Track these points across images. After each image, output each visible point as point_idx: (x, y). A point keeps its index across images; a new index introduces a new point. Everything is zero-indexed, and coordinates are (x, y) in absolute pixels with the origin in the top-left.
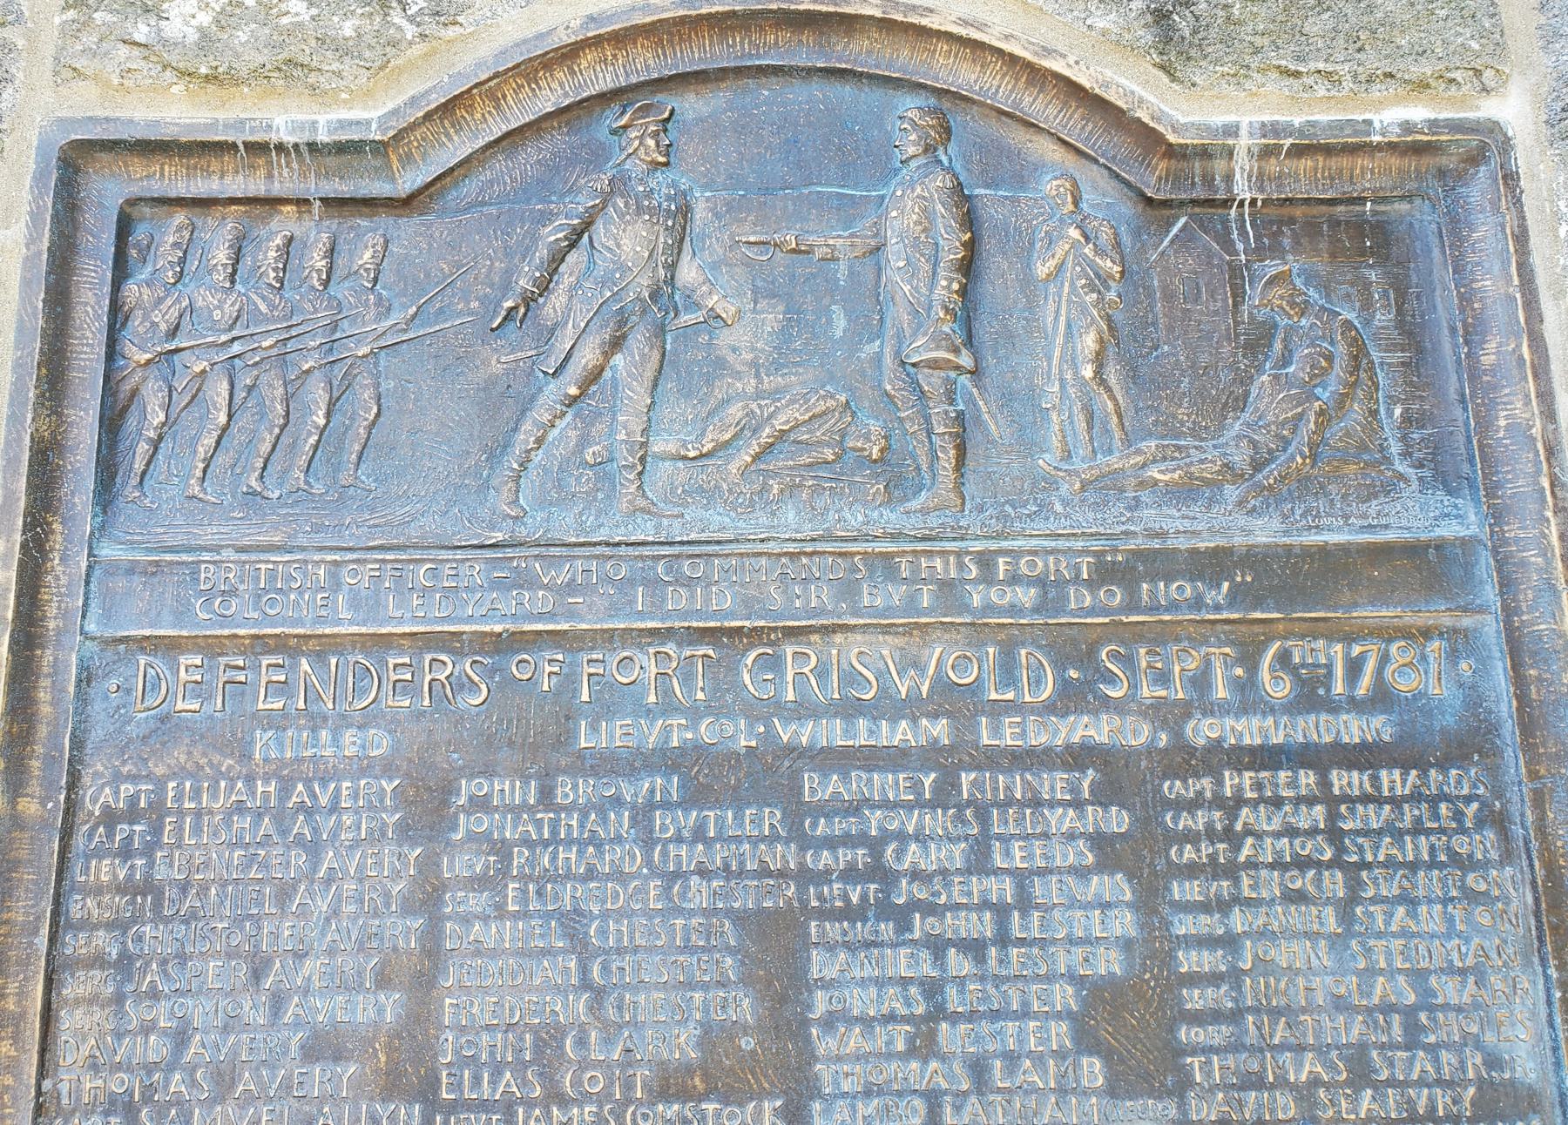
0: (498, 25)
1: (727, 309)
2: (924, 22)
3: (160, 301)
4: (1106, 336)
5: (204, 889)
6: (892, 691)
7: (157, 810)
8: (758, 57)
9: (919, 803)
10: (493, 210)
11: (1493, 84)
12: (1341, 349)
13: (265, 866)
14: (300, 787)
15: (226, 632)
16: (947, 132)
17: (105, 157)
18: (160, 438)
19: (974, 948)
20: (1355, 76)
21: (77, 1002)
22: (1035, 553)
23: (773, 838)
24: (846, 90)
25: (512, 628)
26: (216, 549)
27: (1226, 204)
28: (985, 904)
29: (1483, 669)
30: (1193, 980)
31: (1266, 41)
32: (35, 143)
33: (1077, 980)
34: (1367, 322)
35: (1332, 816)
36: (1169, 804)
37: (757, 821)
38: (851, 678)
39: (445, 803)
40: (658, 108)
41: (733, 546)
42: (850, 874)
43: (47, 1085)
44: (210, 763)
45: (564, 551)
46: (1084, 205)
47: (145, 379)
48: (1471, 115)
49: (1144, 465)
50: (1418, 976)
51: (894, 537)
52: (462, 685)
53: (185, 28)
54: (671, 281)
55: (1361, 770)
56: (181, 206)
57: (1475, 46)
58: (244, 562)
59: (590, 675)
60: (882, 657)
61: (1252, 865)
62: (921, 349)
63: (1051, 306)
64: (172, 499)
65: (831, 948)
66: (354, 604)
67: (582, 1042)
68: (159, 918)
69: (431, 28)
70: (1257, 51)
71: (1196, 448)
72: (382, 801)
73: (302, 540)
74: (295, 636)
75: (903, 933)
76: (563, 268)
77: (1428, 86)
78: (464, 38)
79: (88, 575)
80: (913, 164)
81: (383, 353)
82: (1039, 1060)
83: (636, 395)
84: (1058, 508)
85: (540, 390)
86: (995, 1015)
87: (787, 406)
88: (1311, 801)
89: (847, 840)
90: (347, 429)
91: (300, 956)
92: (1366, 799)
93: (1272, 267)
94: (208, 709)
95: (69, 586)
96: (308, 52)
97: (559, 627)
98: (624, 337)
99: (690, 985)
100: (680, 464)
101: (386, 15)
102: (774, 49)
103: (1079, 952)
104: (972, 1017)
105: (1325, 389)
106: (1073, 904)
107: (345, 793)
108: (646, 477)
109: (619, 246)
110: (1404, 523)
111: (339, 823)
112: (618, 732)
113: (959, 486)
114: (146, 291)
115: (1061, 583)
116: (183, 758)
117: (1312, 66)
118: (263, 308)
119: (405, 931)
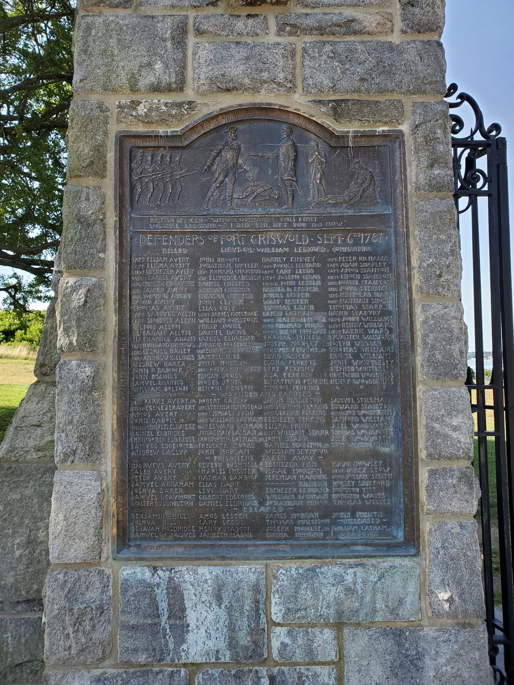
1: (248, 169)
3: (139, 167)
5: (155, 276)
7: (145, 263)
9: (283, 263)
10: (202, 149)
12: (368, 177)
13: (166, 272)
17: (127, 138)
19: (292, 287)
20: (373, 121)
21: (135, 294)
22: (306, 217)
23: (256, 269)
24: (272, 124)
26: (153, 215)
28: (294, 280)
29: (390, 239)
30: (331, 293)
31: (356, 113)
33: (310, 293)
34: (374, 171)
35: (359, 265)
37: (253, 266)
39: (198, 262)
40: (234, 127)
42: (270, 275)
43: (131, 307)
49: (328, 200)
50: (372, 292)
51: (280, 214)
54: (237, 163)
57: (397, 115)
61: (343, 273)
63: (312, 168)
65: (267, 287)
67: (223, 302)
68: (148, 281)
70: (354, 115)
73: (169, 214)
78: (195, 114)
82: (303, 305)
83: (230, 186)
86: (295, 298)
88: (355, 262)
89: (270, 269)
91: (173, 287)
92: (365, 262)
93: (356, 160)
94: (153, 245)
99: (242, 293)
102: (257, 115)
104: (291, 298)
106: (310, 280)
115: (311, 222)
119: (192, 283)
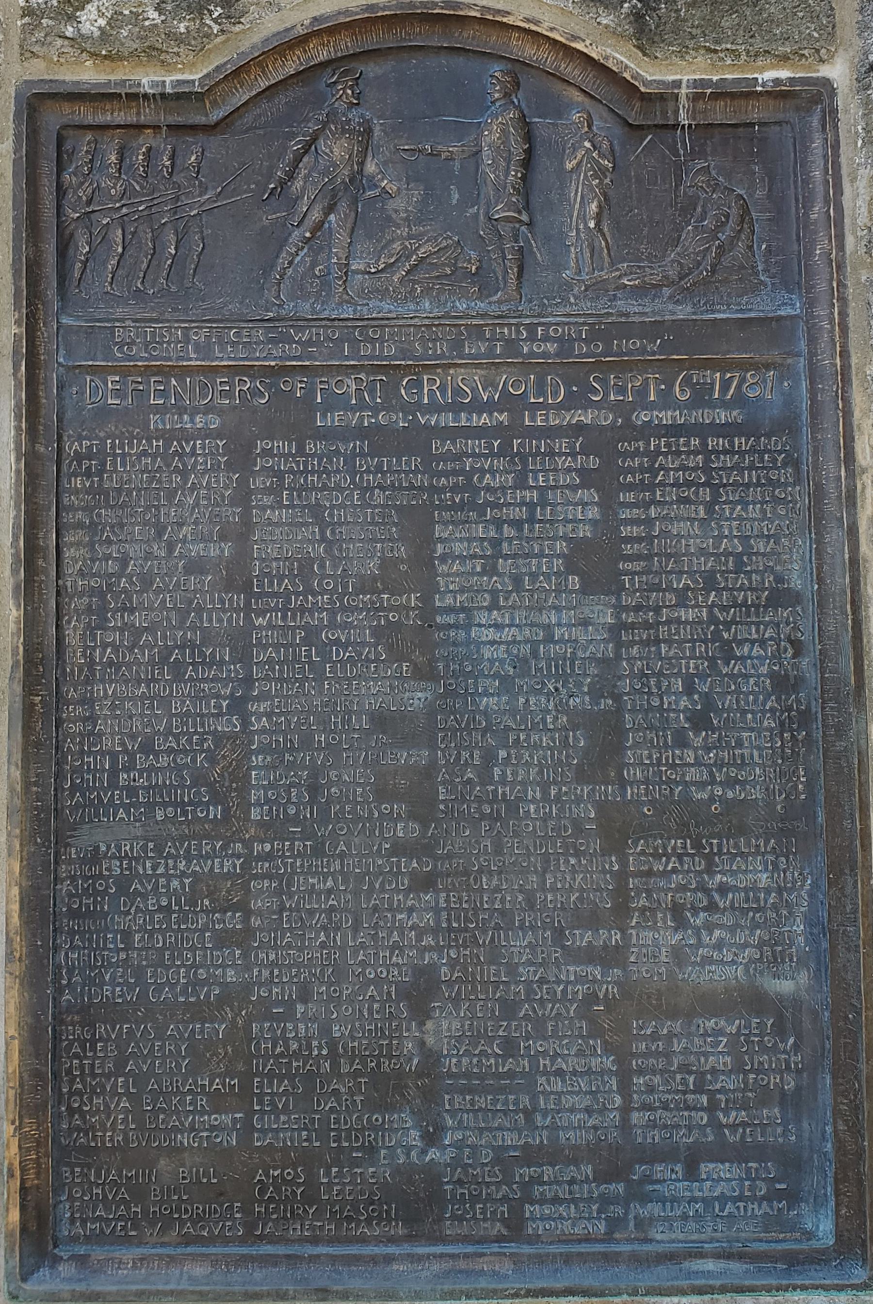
0: (263, 23)
1: (392, 188)
2: (505, 20)
3: (82, 183)
4: (603, 204)
5: (129, 492)
6: (479, 399)
8: (410, 41)
9: (492, 455)
11: (826, 57)
12: (734, 212)
13: (159, 481)
14: (175, 443)
15: (132, 364)
16: (517, 84)
17: (49, 102)
18: (87, 260)
19: (517, 524)
20: (748, 52)
21: (72, 544)
23: (416, 472)
24: (460, 61)
25: (280, 364)
26: (122, 320)
27: (675, 127)
28: (523, 503)
30: (629, 540)
31: (699, 31)
32: (13, 95)
34: (751, 196)
35: (707, 460)
36: (620, 454)
38: (458, 392)
39: (251, 452)
41: (396, 321)
42: (455, 489)
43: (60, 582)
44: (128, 431)
45: (306, 323)
46: (594, 128)
47: (76, 228)
48: (814, 75)
49: (620, 277)
50: (744, 539)
51: (483, 316)
52: (255, 393)
53: (92, 28)
54: (361, 171)
55: (724, 438)
56: (90, 130)
57: (816, 35)
58: (138, 327)
59: (321, 389)
60: (475, 381)
61: (662, 484)
62: (500, 211)
63: (573, 186)
64: (96, 293)
65: (446, 524)
66: (197, 348)
67: (322, 566)
68: (108, 506)
69: (227, 26)
70: (693, 37)
71: (648, 267)
72: (218, 451)
73: (167, 316)
74: (168, 366)
75: (481, 517)
76: (301, 165)
77: (789, 58)
78: (243, 32)
79: (58, 333)
80: (498, 104)
81: (204, 214)
82: (547, 576)
83: (341, 237)
84: (572, 300)
85: (290, 235)
86: (527, 556)
87: (425, 243)
88: (696, 453)
89: (455, 473)
90: (188, 255)
91: (181, 525)
92: (725, 452)
93: (700, 164)
94: (125, 403)
95: (48, 338)
96: (160, 41)
97: (304, 364)
98: (335, 204)
100: (367, 276)
101: (202, 19)
103: (570, 526)
104: (515, 556)
105: (723, 234)
106: (569, 503)
107: (198, 446)
108: (348, 284)
109: (332, 152)
110: (761, 308)
111: (196, 461)
112: (337, 419)
113: (519, 287)
114: (74, 179)
115: (572, 340)
116: (113, 429)
117: (724, 46)
118: (138, 188)
119: (233, 514)
